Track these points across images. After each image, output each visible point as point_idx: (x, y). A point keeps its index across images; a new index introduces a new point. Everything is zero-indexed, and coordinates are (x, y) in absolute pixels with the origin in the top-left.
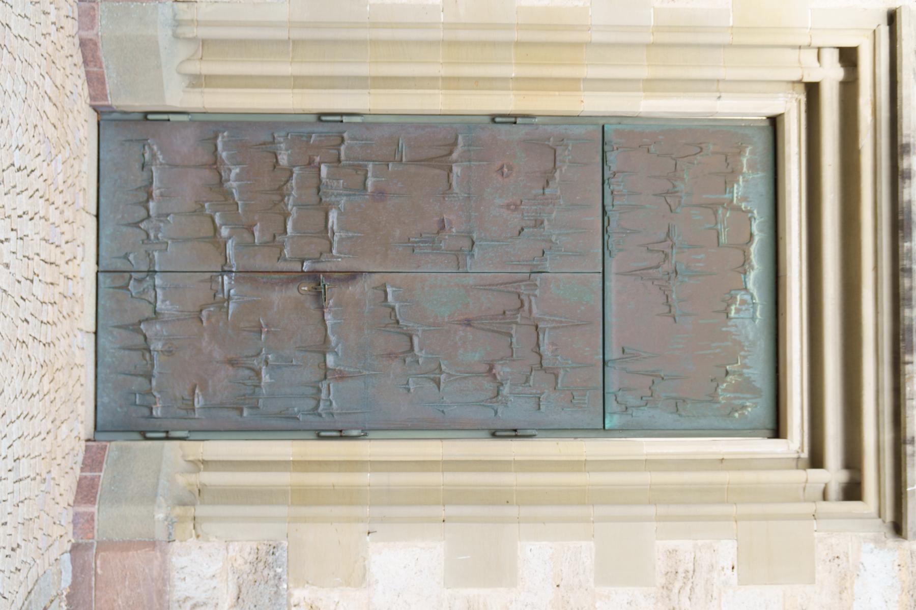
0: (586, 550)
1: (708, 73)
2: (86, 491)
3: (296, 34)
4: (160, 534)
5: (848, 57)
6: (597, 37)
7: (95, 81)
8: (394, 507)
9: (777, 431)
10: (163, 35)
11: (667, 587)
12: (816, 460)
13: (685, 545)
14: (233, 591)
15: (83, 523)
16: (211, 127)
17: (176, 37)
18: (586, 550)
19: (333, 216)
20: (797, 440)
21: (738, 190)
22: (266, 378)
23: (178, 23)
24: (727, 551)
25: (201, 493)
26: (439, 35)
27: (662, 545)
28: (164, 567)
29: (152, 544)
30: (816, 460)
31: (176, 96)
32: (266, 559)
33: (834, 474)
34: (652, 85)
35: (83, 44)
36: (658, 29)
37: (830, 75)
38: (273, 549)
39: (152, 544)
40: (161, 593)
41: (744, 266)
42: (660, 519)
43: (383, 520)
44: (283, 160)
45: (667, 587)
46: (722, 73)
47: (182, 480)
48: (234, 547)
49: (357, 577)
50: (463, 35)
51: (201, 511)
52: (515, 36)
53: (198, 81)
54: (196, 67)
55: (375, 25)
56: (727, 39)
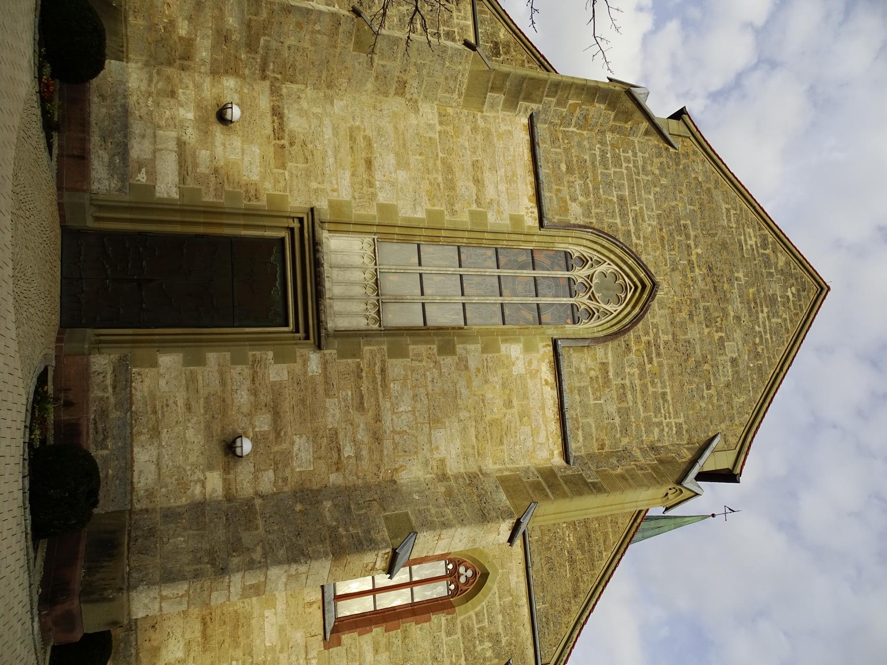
0: (228, 355)
1: (261, 223)
2: (59, 340)
3: (132, 205)
4: (86, 352)
5: (301, 220)
6: (227, 211)
7: (62, 217)
8: (166, 345)
9: (287, 325)
10: (87, 203)
11: (253, 365)
12: (297, 331)
13: (258, 353)
14: (112, 368)
15: (58, 349)
16: (102, 235)
17: (91, 204)
18: (228, 355)
19: (144, 263)
20: (291, 327)
21: (272, 259)
22: (122, 311)
23: (92, 199)
24: (270, 354)
25: (100, 342)
26: (178, 207)
27: (251, 353)
28: (88, 361)
29: (84, 354)
30: (297, 331)
31: (91, 224)
32: (123, 360)
33: (301, 334)
34: (246, 226)
35: (59, 204)
36: (245, 209)
37: (296, 225)
38: (126, 356)
39: (84, 354)
40: (87, 370)
41: (275, 280)
42: (250, 345)
43: (163, 347)
44: (127, 245)
45: (253, 365)
46: (266, 224)
47: (93, 339)
48: (112, 356)
49: (154, 364)
50: (186, 208)
51: (100, 345)
52: (202, 209)
53: (97, 219)
54: (97, 214)
55: (158, 204)
56: (266, 213)
